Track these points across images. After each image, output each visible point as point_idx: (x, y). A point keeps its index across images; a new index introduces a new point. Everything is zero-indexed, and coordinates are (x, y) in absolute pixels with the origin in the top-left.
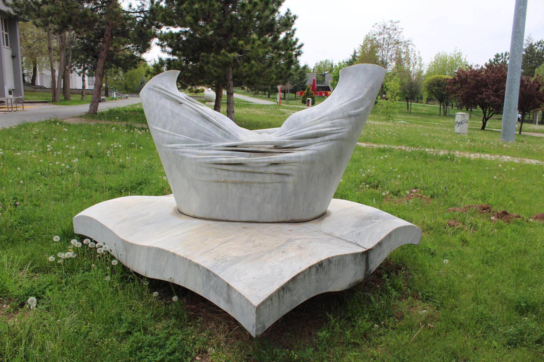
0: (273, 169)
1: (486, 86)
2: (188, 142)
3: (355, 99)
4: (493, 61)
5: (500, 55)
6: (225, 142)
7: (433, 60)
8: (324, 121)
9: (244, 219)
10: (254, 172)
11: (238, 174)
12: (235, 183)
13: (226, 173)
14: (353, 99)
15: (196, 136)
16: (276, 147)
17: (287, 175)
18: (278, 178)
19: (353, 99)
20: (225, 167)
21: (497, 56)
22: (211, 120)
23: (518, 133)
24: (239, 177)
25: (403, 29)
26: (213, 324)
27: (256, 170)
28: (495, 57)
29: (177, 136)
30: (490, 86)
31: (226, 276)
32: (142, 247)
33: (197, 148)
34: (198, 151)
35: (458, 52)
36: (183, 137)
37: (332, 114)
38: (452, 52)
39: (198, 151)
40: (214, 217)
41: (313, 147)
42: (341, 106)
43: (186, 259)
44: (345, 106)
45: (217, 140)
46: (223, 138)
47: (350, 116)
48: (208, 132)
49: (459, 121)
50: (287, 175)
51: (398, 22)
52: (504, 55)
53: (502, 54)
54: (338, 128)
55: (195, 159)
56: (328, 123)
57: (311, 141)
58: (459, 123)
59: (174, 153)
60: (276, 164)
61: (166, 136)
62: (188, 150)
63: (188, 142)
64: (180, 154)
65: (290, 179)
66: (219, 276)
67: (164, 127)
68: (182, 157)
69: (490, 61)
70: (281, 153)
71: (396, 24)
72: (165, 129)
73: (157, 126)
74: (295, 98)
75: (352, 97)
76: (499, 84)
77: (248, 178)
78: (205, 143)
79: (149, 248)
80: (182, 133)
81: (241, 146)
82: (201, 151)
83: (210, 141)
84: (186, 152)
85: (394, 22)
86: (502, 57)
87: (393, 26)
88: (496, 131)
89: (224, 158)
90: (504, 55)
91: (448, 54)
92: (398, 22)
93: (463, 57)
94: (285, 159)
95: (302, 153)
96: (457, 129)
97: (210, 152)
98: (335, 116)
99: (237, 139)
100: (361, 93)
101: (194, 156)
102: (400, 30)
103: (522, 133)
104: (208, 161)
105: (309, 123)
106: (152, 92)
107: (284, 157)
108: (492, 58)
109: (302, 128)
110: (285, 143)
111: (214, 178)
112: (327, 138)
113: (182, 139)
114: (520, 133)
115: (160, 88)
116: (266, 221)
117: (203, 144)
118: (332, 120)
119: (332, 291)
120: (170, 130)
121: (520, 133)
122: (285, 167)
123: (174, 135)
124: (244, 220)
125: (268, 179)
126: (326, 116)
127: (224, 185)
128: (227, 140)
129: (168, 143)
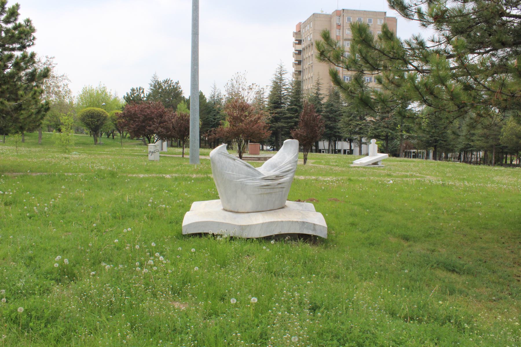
0: (280, 186)
1: (151, 119)
2: (246, 178)
4: (130, 94)
5: (135, 89)
7: (81, 93)
8: (288, 164)
9: (269, 209)
10: (274, 188)
11: (269, 190)
12: (267, 194)
13: (265, 190)
15: (248, 175)
16: (277, 177)
17: (284, 188)
18: (281, 189)
20: (265, 187)
21: (133, 90)
23: (181, 156)
24: (269, 191)
25: (57, 64)
26: (147, 304)
27: (275, 187)
28: (131, 91)
35: (102, 86)
36: (243, 176)
38: (97, 86)
40: (258, 210)
41: (289, 175)
49: (152, 150)
50: (284, 188)
51: (54, 58)
52: (138, 89)
53: (137, 89)
55: (253, 185)
57: (287, 173)
58: (153, 152)
60: (280, 184)
61: (235, 176)
65: (284, 189)
67: (233, 172)
68: (246, 185)
69: (127, 94)
71: (51, 60)
73: (228, 171)
76: (162, 117)
77: (271, 191)
83: (254, 176)
85: (49, 57)
86: (137, 91)
87: (48, 61)
88: (169, 157)
90: (138, 89)
91: (94, 87)
92: (54, 58)
93: (108, 91)
96: (151, 157)
97: (256, 181)
99: (263, 175)
101: (252, 184)
102: (53, 65)
103: (185, 156)
104: (259, 185)
106: (220, 155)
108: (129, 91)
110: (280, 175)
111: (260, 192)
114: (183, 156)
115: (224, 153)
121: (183, 156)
122: (284, 184)
125: (278, 190)
127: (262, 195)
129: (237, 179)
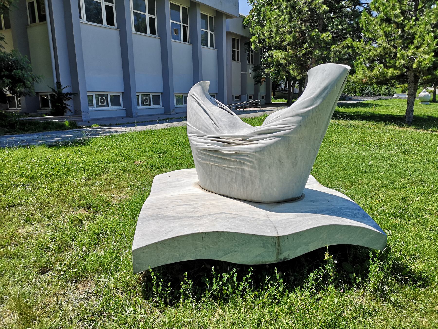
45: (211, 132)
47: (297, 115)
48: (207, 126)
70: (242, 144)
98: (287, 115)
100: (313, 93)
116: (234, 197)
126: (281, 115)
128: (216, 133)
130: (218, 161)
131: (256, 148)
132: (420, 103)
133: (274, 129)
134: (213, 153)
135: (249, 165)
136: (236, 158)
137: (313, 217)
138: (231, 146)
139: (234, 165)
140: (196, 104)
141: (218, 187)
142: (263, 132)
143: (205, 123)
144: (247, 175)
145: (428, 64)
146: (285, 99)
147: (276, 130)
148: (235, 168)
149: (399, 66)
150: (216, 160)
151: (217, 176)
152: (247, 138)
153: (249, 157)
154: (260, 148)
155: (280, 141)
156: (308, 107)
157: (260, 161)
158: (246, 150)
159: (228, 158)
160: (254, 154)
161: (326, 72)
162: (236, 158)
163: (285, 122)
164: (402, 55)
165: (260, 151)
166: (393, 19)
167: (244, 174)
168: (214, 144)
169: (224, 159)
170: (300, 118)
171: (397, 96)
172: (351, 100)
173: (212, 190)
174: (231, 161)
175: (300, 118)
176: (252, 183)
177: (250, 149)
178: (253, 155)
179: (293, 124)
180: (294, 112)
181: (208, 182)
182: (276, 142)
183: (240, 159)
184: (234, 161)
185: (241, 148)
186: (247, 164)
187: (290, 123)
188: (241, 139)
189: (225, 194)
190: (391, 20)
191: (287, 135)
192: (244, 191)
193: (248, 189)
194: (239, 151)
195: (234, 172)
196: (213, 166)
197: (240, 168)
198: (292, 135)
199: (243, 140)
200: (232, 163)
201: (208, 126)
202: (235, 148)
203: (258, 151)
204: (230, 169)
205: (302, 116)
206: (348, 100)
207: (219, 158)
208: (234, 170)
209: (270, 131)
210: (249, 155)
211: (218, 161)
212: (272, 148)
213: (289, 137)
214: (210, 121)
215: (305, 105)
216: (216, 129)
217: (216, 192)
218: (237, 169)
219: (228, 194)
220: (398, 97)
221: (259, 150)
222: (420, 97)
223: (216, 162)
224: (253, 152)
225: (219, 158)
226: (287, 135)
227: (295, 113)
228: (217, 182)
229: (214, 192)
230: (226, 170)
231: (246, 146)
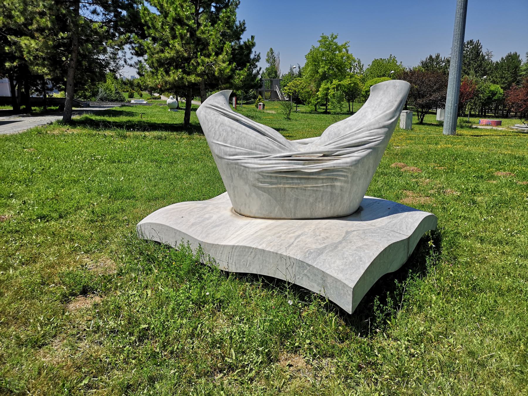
2: (248, 154)
3: (388, 112)
6: (281, 152)
14: (385, 112)
19: (385, 112)
22: (267, 134)
29: (239, 149)
30: (170, 46)
31: (319, 264)
32: (225, 246)
33: (258, 159)
34: (259, 162)
36: (243, 150)
37: (370, 125)
39: (259, 162)
41: (356, 154)
42: (377, 118)
43: (277, 253)
44: (380, 118)
45: (274, 151)
46: (279, 149)
47: (384, 127)
48: (266, 145)
54: (375, 137)
56: (367, 133)
59: (237, 164)
62: (250, 161)
63: (248, 154)
64: (243, 164)
66: (314, 265)
70: (330, 160)
72: (226, 143)
74: (316, 110)
75: (385, 109)
78: (264, 154)
79: (233, 247)
80: (243, 147)
81: (296, 155)
82: (262, 162)
84: (251, 163)
89: (283, 167)
94: (335, 165)
95: (348, 160)
98: (372, 127)
100: (392, 106)
101: (256, 166)
105: (350, 133)
106: (209, 110)
107: (334, 164)
109: (344, 139)
112: (367, 146)
113: (243, 151)
116: (317, 217)
117: (263, 156)
118: (370, 130)
119: (390, 272)
120: (231, 144)
123: (235, 148)
124: (299, 217)
126: (364, 127)
128: (283, 151)
129: (230, 155)
130: (299, 182)
131: (352, 162)
132: (169, 110)
133: (365, 141)
134: (292, 174)
135: (343, 180)
136: (328, 175)
137: (400, 217)
138: (315, 163)
139: (323, 183)
140: (226, 119)
141: (293, 211)
142: (353, 145)
143: (260, 141)
144: (338, 191)
145: (229, 72)
146: (8, 105)
147: (366, 143)
148: (323, 186)
149: (200, 72)
150: (296, 181)
151: (293, 200)
152: (332, 152)
153: (345, 172)
154: (355, 161)
155: (371, 152)
156: (391, 119)
157: (354, 173)
158: (342, 165)
159: (316, 177)
160: (350, 167)
161: (398, 88)
162: (328, 175)
163: (372, 133)
164: (203, 61)
165: (356, 164)
166: (185, 21)
167: (334, 191)
168: (289, 163)
169: (308, 179)
170: (386, 130)
171: (135, 102)
172: (88, 106)
173: (284, 216)
174: (319, 179)
175: (386, 130)
176: (342, 198)
177: (347, 163)
178: (349, 169)
179: (381, 136)
180: (380, 124)
181: (276, 209)
182: (369, 154)
183: (333, 175)
184: (324, 178)
185: (336, 164)
186: (340, 180)
187: (378, 134)
188: (322, 155)
189: (303, 217)
190: (183, 21)
191: (377, 146)
192: (331, 209)
193: (336, 205)
194: (334, 167)
195: (320, 191)
196: (287, 190)
197: (329, 185)
198: (380, 146)
199: (324, 156)
200: (320, 181)
201: (268, 144)
202: (327, 165)
203: (354, 165)
204: (315, 189)
205: (388, 128)
206: (86, 107)
207: (301, 179)
208: (321, 189)
209: (360, 144)
210: (344, 170)
211: (299, 182)
212: (365, 160)
213: (378, 148)
214: (265, 139)
215: (389, 117)
216: (280, 147)
217: (290, 218)
218: (325, 187)
219: (308, 215)
220: (136, 103)
221: (355, 163)
222: (169, 104)
223: (296, 183)
224: (350, 166)
225: (301, 179)
226: (377, 146)
227: (381, 125)
228: (291, 205)
229: (286, 217)
230: (309, 190)
231: (335, 162)
